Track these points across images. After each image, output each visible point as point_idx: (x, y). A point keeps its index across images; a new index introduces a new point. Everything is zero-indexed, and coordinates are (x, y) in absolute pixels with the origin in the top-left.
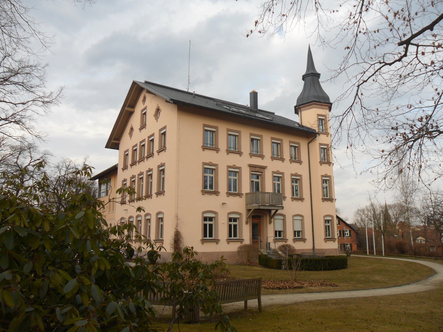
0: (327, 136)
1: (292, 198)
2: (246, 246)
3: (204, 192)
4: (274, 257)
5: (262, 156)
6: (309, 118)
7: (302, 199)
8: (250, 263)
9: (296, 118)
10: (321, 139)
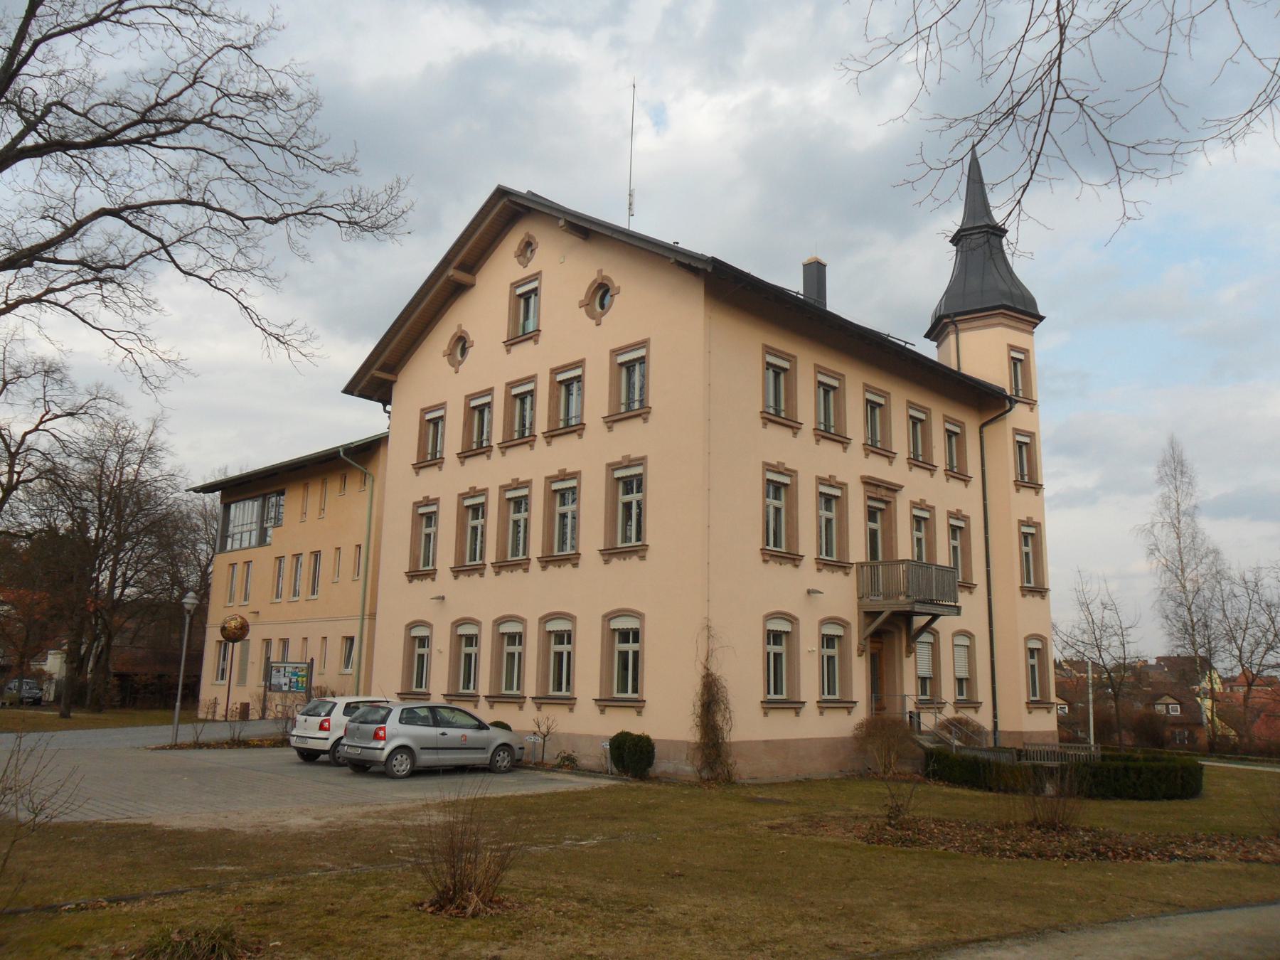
1: (1022, 588)
6: (981, 353)
9: (928, 349)
10: (1018, 416)
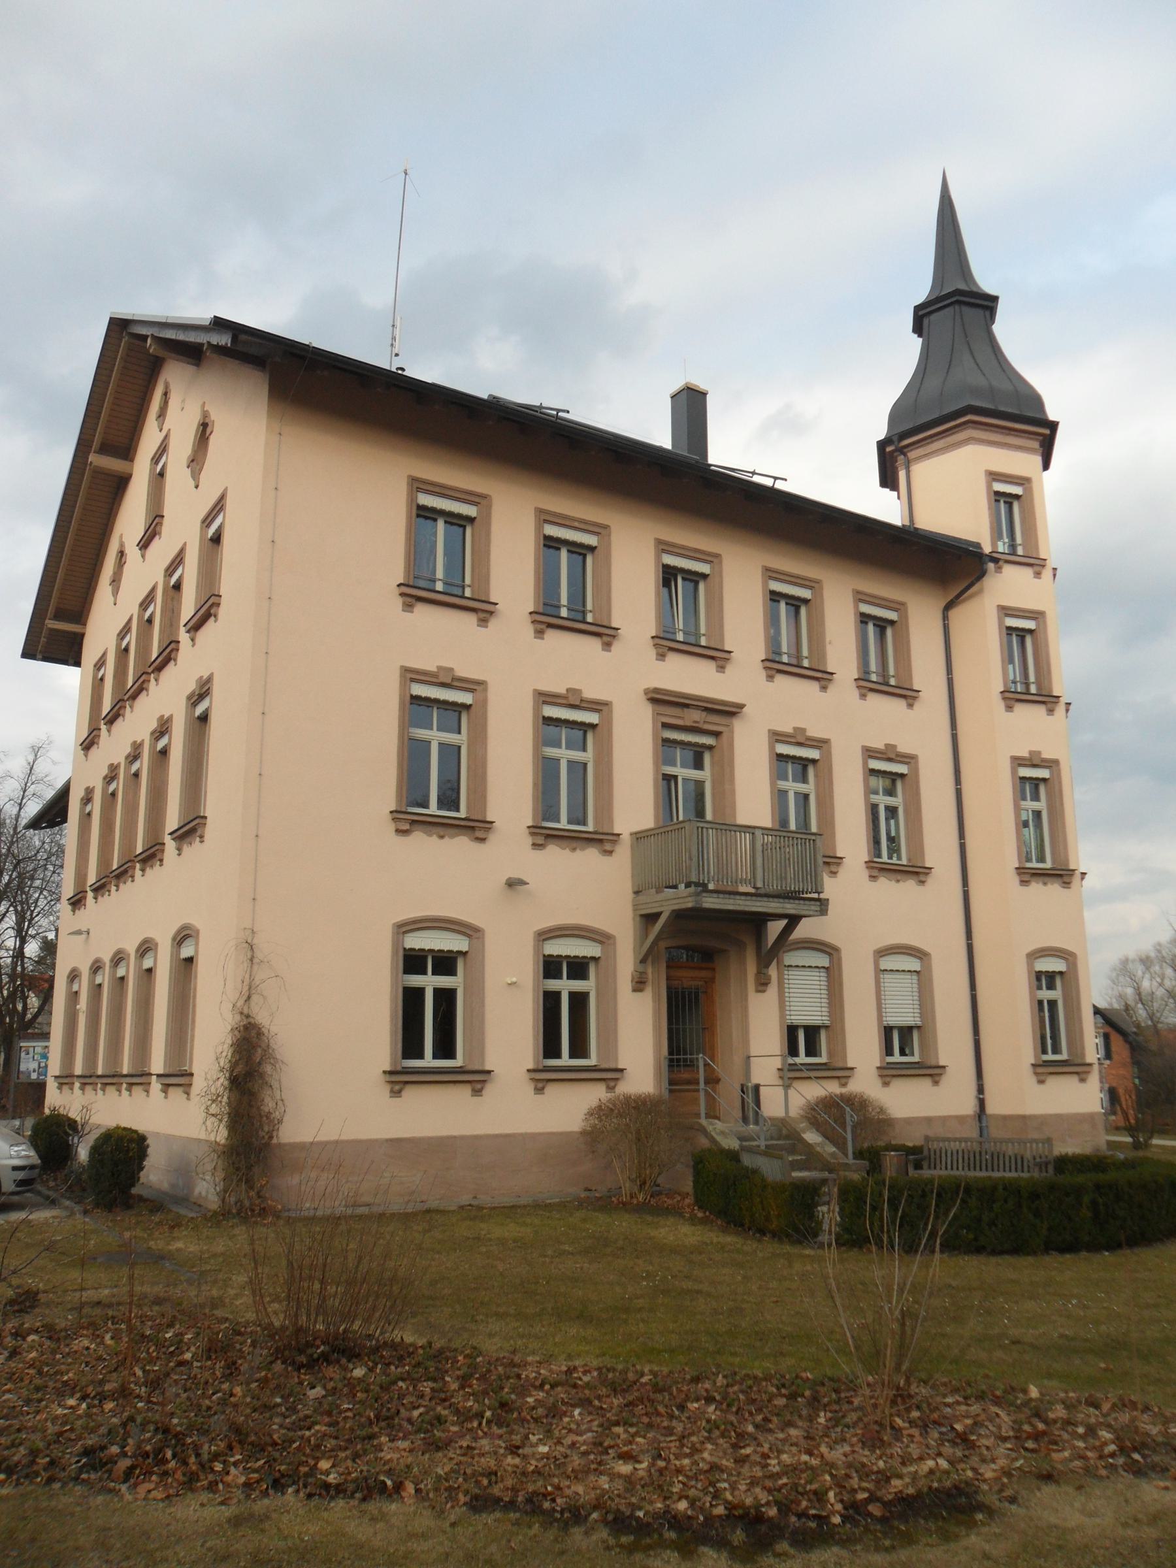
0: (1038, 575)
2: (637, 1106)
3: (409, 818)
4: (771, 1170)
5: (718, 656)
6: (950, 493)
7: (918, 872)
8: (652, 1202)
9: (885, 507)
10: (1008, 586)
